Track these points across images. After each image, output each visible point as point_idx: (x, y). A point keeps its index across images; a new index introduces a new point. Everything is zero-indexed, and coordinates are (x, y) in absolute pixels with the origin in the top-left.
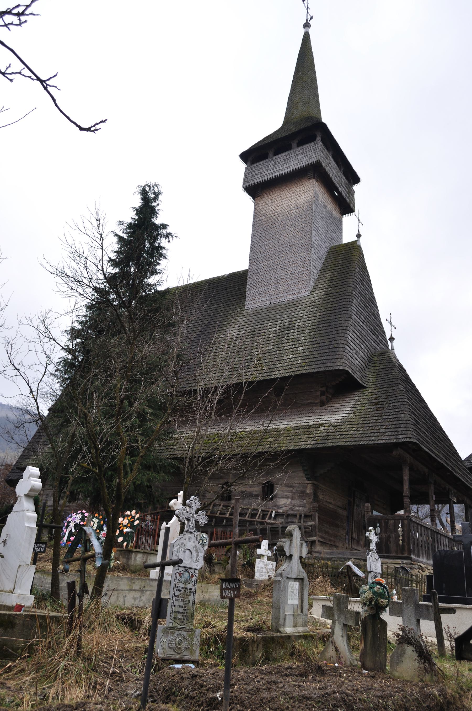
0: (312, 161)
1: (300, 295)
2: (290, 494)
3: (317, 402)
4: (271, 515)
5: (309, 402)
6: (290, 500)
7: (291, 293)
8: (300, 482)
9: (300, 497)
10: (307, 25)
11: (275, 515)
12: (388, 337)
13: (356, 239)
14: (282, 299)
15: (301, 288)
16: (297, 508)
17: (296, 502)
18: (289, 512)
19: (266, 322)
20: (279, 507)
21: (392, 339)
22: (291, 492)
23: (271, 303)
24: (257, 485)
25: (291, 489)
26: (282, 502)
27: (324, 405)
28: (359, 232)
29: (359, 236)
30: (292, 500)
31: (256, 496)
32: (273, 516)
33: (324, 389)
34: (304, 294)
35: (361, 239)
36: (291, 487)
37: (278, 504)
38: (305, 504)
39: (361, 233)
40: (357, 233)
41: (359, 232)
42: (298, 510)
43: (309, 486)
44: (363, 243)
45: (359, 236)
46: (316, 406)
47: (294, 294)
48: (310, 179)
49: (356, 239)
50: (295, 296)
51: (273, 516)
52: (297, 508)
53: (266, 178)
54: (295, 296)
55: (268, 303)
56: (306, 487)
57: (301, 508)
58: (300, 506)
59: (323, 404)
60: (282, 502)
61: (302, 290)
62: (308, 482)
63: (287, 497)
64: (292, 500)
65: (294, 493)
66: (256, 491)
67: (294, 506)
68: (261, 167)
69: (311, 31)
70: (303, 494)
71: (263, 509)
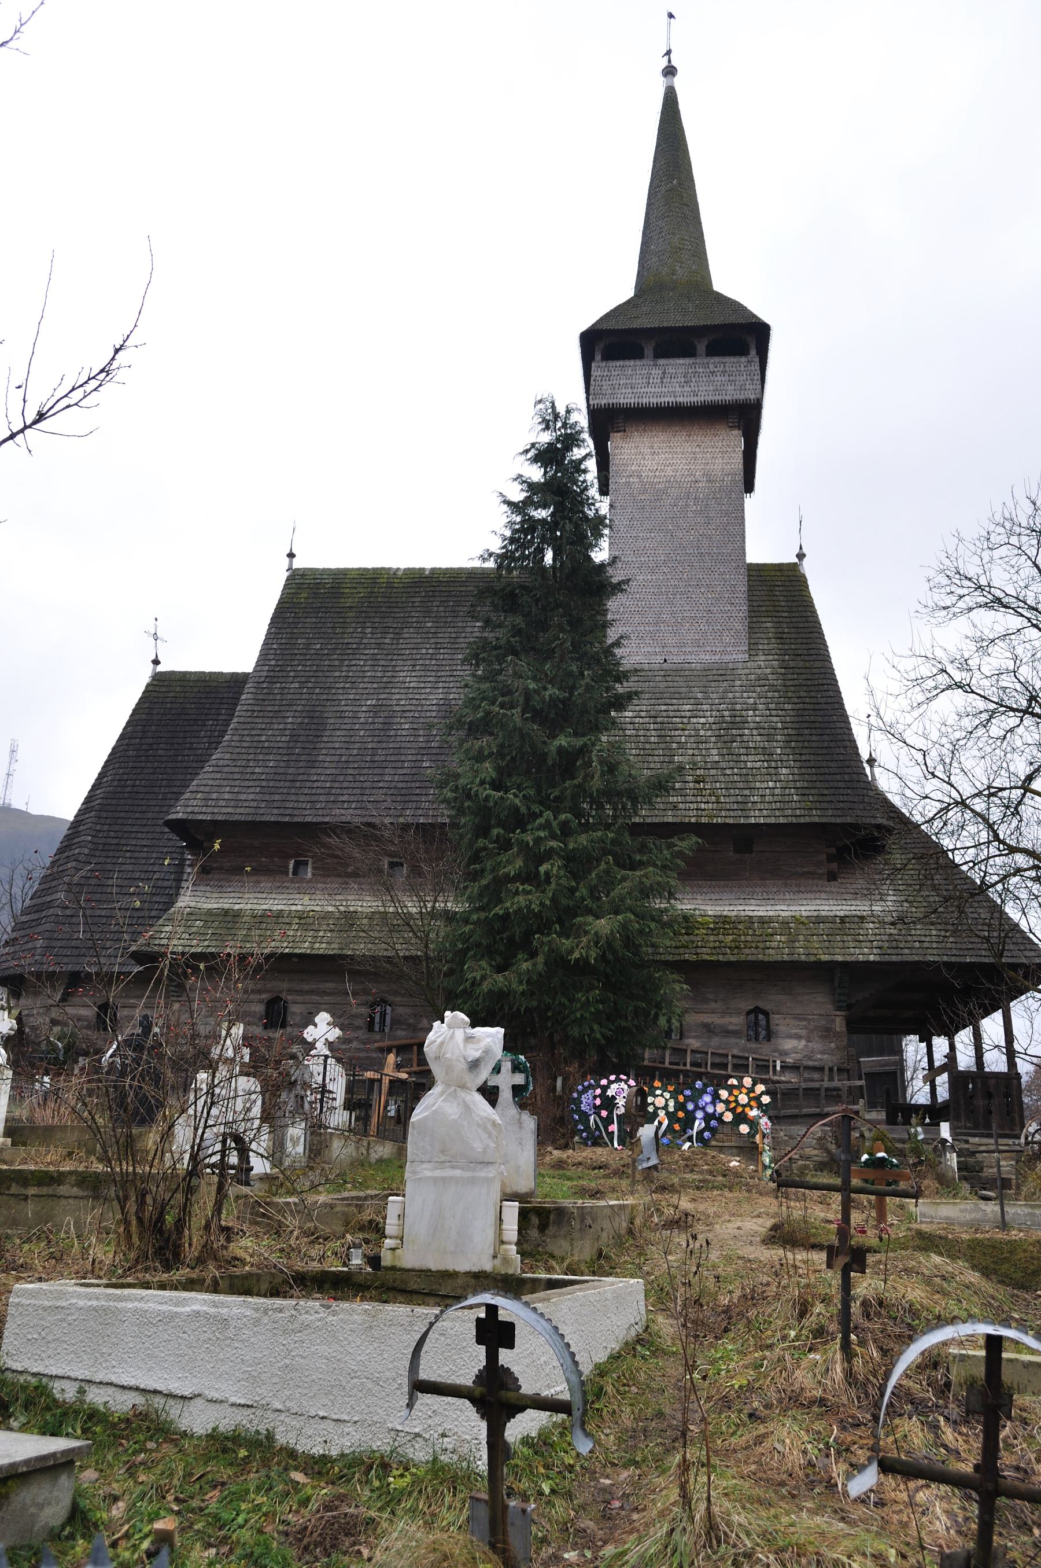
0: (746, 396)
1: (727, 657)
2: (804, 1032)
3: (821, 871)
4: (775, 1067)
5: (806, 870)
6: (803, 1043)
7: (708, 648)
8: (822, 1012)
9: (821, 1037)
10: (670, 71)
11: (781, 1067)
12: (865, 755)
13: (796, 560)
14: (690, 658)
15: (728, 645)
16: (819, 1056)
17: (816, 1045)
18: (805, 1063)
19: (675, 701)
20: (786, 1053)
21: (871, 761)
22: (806, 1028)
23: (665, 661)
24: (739, 1014)
25: (804, 1023)
26: (789, 1044)
27: (835, 880)
28: (801, 548)
29: (801, 556)
30: (808, 1041)
31: (736, 1033)
32: (778, 1068)
33: (833, 851)
34: (735, 656)
35: (805, 561)
36: (804, 1019)
37: (781, 1048)
38: (833, 1050)
39: (805, 550)
40: (797, 551)
41: (801, 548)
42: (821, 1060)
43: (838, 1020)
44: (808, 568)
45: (801, 556)
46: (819, 878)
47: (714, 653)
48: (732, 428)
49: (796, 560)
50: (717, 657)
51: (778, 1068)
52: (819, 1056)
53: (645, 401)
54: (717, 657)
55: (659, 659)
56: (834, 1021)
57: (825, 1056)
58: (823, 1053)
59: (832, 877)
60: (789, 1044)
61: (731, 648)
62: (838, 1013)
63: (798, 1037)
64: (808, 1041)
65: (811, 1031)
66: (735, 1025)
67: (812, 1052)
68: (630, 372)
69: (678, 82)
70: (827, 1033)
71: (755, 1056)
